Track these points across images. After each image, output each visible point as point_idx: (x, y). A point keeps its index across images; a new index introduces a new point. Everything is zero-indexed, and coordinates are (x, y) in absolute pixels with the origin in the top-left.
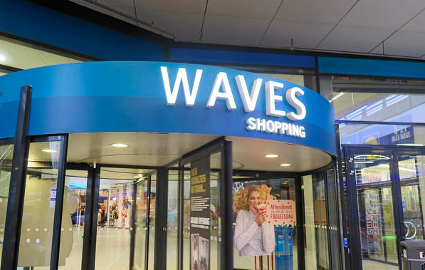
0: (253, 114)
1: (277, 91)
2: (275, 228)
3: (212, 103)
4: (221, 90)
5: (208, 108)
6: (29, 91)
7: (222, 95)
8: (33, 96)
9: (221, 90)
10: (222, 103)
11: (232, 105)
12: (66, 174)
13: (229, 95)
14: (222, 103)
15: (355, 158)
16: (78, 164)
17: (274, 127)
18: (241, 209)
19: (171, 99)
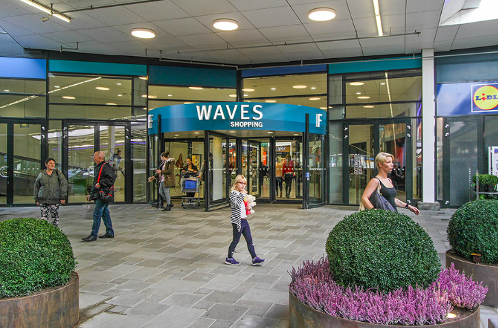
0: (234, 120)
1: (245, 109)
2: (404, 113)
3: (215, 118)
4: (219, 112)
5: (395, 197)
6: (160, 116)
7: (219, 114)
8: (162, 118)
9: (219, 112)
10: (219, 117)
11: (224, 118)
12: (100, 130)
13: (222, 114)
14: (219, 117)
15: (284, 182)
16: (344, 194)
17: (245, 124)
18: (293, 281)
19: (200, 118)
